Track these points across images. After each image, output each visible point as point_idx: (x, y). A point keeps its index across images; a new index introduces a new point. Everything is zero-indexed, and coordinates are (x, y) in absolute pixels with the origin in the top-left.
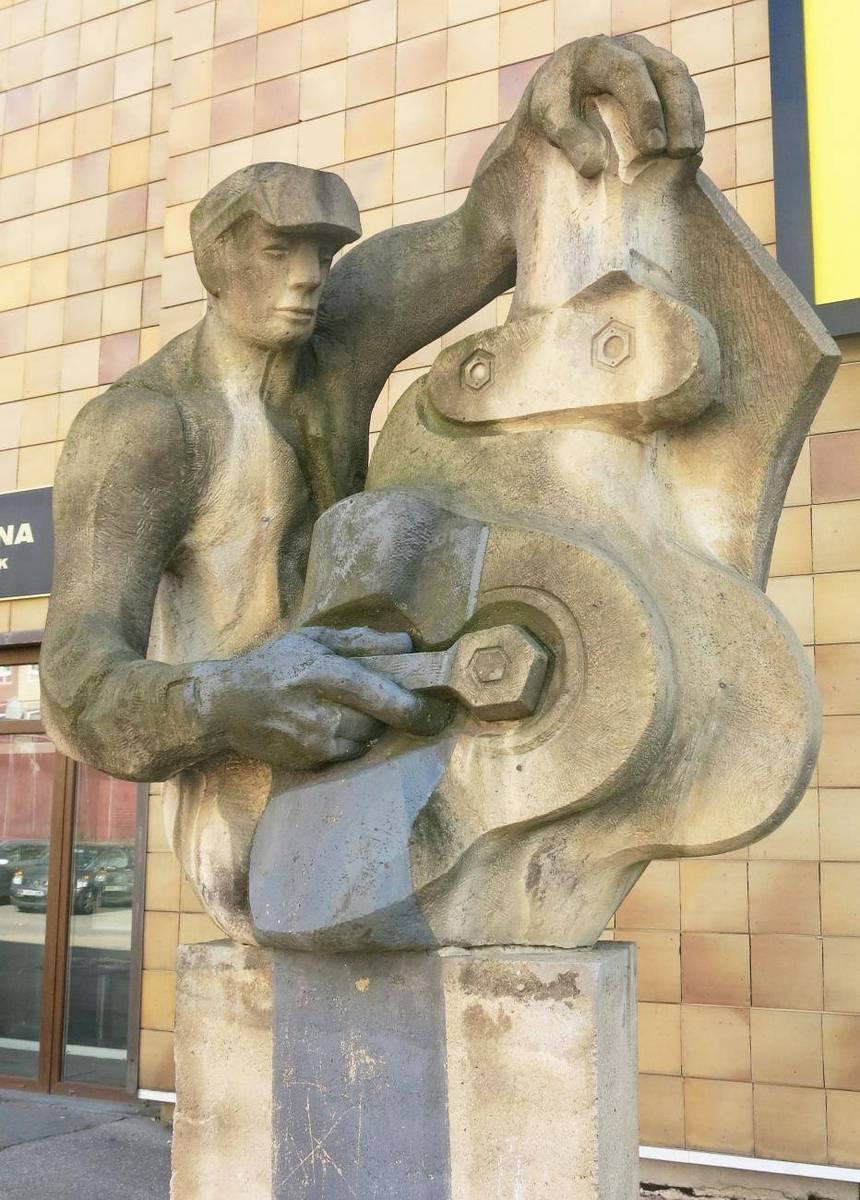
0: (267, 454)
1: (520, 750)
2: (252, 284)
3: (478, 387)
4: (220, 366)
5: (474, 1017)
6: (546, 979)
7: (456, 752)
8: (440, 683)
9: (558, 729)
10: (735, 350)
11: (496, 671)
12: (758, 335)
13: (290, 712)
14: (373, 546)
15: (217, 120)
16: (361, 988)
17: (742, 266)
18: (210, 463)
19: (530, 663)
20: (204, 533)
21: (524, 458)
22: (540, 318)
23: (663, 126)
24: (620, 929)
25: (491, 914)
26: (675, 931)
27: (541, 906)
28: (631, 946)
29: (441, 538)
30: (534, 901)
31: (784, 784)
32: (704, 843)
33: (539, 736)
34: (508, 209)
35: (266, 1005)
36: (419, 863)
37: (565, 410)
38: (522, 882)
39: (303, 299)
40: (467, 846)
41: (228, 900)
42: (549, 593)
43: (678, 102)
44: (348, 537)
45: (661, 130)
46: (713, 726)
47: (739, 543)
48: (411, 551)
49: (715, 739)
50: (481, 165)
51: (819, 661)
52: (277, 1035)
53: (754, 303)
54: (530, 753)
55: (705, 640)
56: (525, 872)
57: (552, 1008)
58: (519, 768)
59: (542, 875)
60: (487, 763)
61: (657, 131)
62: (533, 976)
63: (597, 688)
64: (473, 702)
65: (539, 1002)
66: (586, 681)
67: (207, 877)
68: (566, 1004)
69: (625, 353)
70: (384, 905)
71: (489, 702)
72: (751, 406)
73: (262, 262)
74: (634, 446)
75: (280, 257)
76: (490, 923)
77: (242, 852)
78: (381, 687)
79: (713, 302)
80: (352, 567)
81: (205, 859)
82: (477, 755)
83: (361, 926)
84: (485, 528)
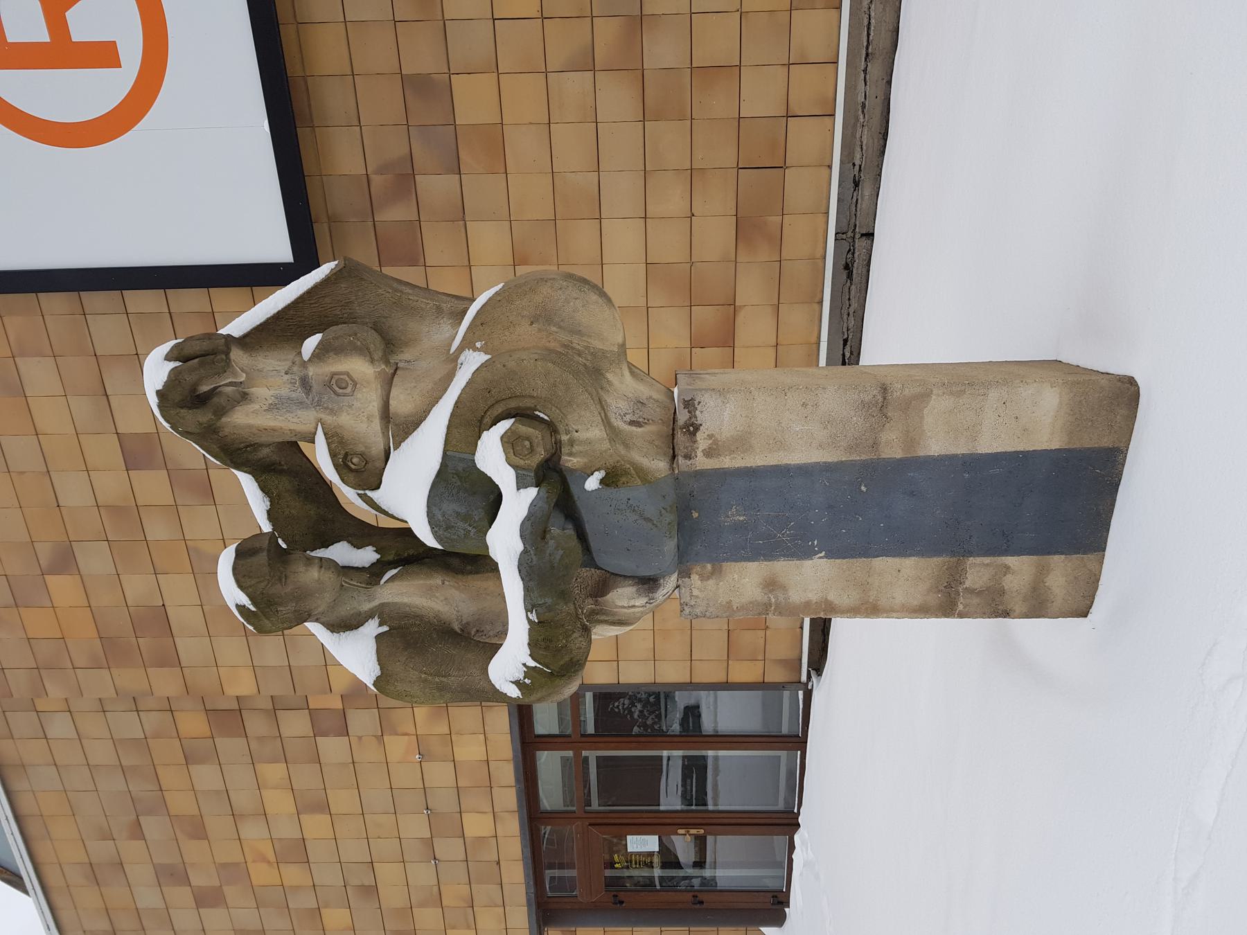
0: (405, 583)
1: (568, 432)
2: (302, 595)
5: (708, 453)
7: (570, 466)
8: (532, 474)
10: (341, 316)
14: (458, 514)
15: (162, 663)
16: (697, 515)
17: (291, 312)
19: (520, 426)
25: (656, 446)
30: (650, 424)
34: (256, 446)
35: (709, 566)
38: (639, 430)
41: (653, 588)
44: (453, 529)
49: (560, 327)
51: (524, 262)
52: (727, 560)
53: (314, 305)
55: (507, 333)
58: (577, 432)
60: (576, 448)
64: (542, 456)
67: (641, 601)
79: (313, 328)
82: (570, 454)
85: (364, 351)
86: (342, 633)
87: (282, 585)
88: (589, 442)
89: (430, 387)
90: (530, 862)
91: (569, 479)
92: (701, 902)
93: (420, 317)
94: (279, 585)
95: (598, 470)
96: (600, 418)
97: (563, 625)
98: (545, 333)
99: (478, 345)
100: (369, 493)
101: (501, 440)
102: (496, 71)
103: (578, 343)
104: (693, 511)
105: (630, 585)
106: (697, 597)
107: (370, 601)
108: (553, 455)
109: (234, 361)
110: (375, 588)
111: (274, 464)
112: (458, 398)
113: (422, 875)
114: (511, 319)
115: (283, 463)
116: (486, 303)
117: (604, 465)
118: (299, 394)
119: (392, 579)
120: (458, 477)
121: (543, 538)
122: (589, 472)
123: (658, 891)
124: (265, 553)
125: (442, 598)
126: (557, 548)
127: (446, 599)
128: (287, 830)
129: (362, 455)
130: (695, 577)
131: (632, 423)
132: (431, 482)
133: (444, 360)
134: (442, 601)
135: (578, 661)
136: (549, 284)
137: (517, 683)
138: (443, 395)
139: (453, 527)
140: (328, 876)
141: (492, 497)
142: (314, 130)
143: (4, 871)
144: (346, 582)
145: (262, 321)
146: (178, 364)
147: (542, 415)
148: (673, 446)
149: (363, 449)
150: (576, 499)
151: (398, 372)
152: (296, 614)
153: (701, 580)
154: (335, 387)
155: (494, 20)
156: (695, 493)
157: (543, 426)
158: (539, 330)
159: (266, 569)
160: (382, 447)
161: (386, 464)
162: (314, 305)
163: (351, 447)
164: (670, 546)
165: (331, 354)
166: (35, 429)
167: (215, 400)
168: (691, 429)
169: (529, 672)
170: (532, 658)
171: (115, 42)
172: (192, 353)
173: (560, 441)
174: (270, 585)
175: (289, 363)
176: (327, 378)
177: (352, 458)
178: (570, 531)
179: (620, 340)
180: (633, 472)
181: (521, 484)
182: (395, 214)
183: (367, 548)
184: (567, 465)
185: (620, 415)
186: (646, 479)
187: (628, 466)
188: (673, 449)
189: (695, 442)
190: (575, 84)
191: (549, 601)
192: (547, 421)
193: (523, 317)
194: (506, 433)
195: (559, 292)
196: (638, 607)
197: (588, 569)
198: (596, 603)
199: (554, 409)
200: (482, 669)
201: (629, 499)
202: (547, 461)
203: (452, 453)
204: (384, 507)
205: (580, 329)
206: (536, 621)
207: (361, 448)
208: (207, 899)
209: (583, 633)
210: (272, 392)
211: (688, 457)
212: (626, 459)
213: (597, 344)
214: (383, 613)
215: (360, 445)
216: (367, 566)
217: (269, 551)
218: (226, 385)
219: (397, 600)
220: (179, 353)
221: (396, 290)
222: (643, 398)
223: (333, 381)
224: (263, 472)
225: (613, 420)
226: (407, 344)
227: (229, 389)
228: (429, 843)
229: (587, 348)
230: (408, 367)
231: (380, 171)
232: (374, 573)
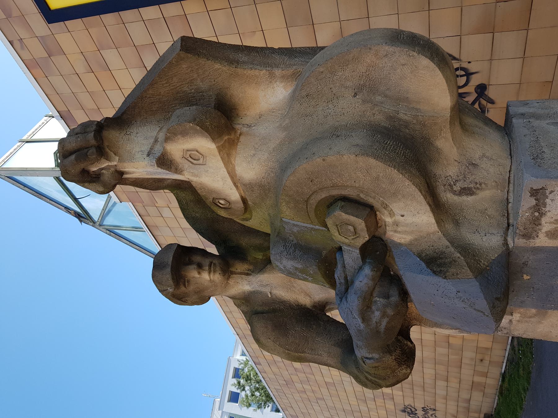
1: (392, 214)
3: (228, 203)
4: (239, 292)
6: (533, 202)
8: (358, 251)
9: (379, 199)
10: (190, 92)
11: (349, 228)
12: (180, 82)
13: (376, 322)
14: (296, 269)
17: (151, 92)
19: (343, 214)
20: (306, 301)
21: (253, 191)
22: (192, 182)
23: (87, 150)
24: (494, 29)
26: (496, 4)
27: (485, 184)
28: (512, 110)
31: (413, 56)
32: (449, 98)
33: (384, 208)
36: (457, 274)
37: (229, 173)
38: (470, 199)
39: (204, 270)
40: (448, 243)
43: (75, 144)
45: (88, 151)
46: (379, 98)
47: (284, 78)
48: (297, 251)
49: (386, 96)
54: (393, 211)
56: (465, 198)
57: (552, 200)
59: (466, 186)
61: (88, 154)
62: (530, 208)
68: (550, 193)
70: (482, 295)
71: (366, 232)
72: (214, 81)
73: (191, 288)
74: (242, 139)
75: (188, 281)
78: (361, 282)
82: (396, 231)
83: (494, 304)
156: (530, 262)
162: (160, 88)
166: (120, 88)
211: (527, 236)
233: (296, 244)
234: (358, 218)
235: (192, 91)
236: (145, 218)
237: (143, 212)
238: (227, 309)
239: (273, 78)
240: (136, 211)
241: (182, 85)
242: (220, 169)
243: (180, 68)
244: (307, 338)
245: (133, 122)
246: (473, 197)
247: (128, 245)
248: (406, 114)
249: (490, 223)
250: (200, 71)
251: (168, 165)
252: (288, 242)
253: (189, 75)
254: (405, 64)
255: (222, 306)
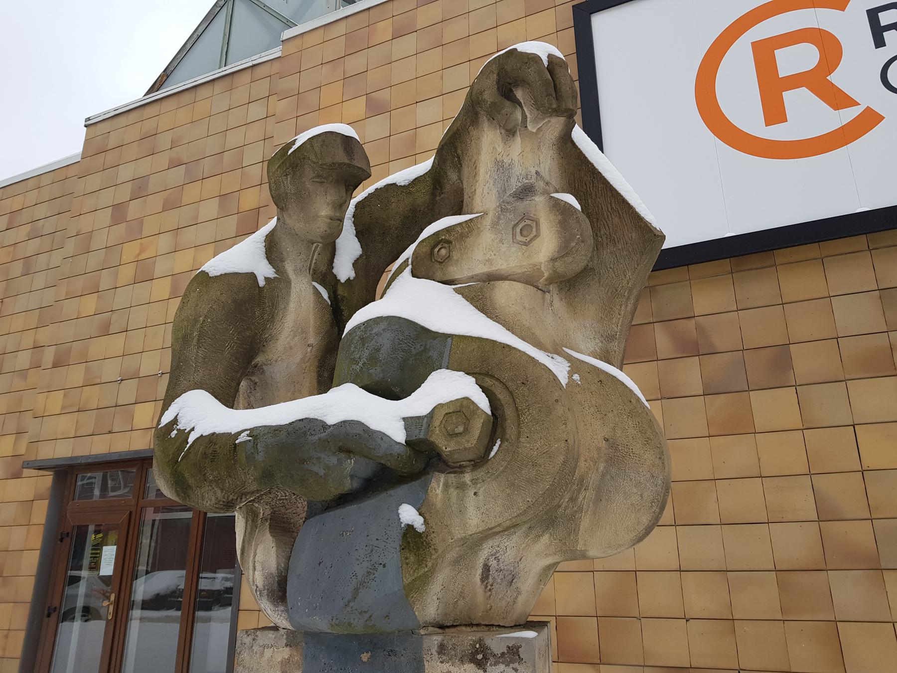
0: (312, 305)
1: (474, 482)
2: (303, 199)
7: (432, 484)
8: (422, 436)
10: (599, 234)
14: (378, 350)
17: (601, 186)
18: (276, 309)
29: (421, 345)
30: (485, 592)
34: (459, 166)
38: (478, 578)
41: (273, 595)
42: (492, 376)
43: (563, 82)
48: (402, 353)
50: (440, 144)
55: (592, 409)
58: (475, 494)
60: (453, 492)
63: (528, 437)
65: (493, 667)
66: (519, 432)
68: (513, 669)
69: (534, 233)
76: (456, 608)
77: (283, 560)
80: (364, 364)
81: (258, 567)
82: (446, 486)
84: (449, 338)
85: (564, 251)
86: (264, 244)
87: (313, 178)
88: (462, 510)
89: (525, 323)
90: (108, 459)
91: (415, 485)
92: (49, 615)
93: (601, 318)
94: (314, 175)
95: (426, 522)
96: (493, 526)
97: (230, 476)
98: (596, 456)
99: (576, 377)
100: (409, 269)
101: (464, 398)
102: (804, 427)
103: (586, 497)
104: (369, 654)
105: (278, 564)
106: (262, 654)
107: (294, 271)
108: (446, 463)
109: (549, 121)
110: (310, 277)
111: (441, 188)
112: (514, 348)
113: (111, 371)
114: (610, 415)
115: (442, 196)
116: (627, 387)
117: (432, 530)
118: (515, 185)
119: (317, 293)
120: (422, 351)
121: (341, 450)
122: (423, 510)
123: (66, 572)
124: (346, 161)
125: (292, 344)
126: (327, 467)
127: (291, 348)
128: (161, 267)
129: (449, 257)
130: (285, 653)
131: (486, 568)
132: (416, 321)
133: (554, 341)
134: (289, 343)
135: (189, 496)
136: (657, 461)
137: (175, 421)
138: (517, 336)
139: (364, 345)
140: (121, 299)
141: (397, 390)
142: (729, 273)
143: (161, 84)
144: (316, 248)
145: (590, 159)
146: (546, 64)
147: (496, 448)
148: (456, 626)
149: (455, 258)
150: (389, 492)
151: (540, 292)
152: (284, 195)
153: (282, 662)
154: (523, 224)
155: (854, 426)
156: (394, 659)
157: (482, 450)
158: (599, 449)
159: (329, 160)
160: (456, 277)
161: (439, 282)
163: (458, 246)
164: (321, 624)
165: (560, 217)
167: (507, 103)
168: (480, 657)
169: (184, 435)
170: (198, 439)
171: (885, 46)
172: (557, 76)
173: (462, 472)
174: (313, 165)
175: (547, 178)
176: (532, 215)
177: (445, 248)
178: (349, 485)
179: (591, 553)
180: (422, 571)
181: (410, 423)
182: (662, 339)
183: (353, 272)
184: (433, 480)
185: (497, 552)
186: (411, 590)
187: (430, 564)
188: (453, 626)
189: (462, 661)
190: (806, 506)
191: (260, 457)
192: (489, 455)
193: (614, 429)
194: (473, 403)
195: (648, 476)
196: (254, 574)
197: (306, 509)
198: (264, 519)
199: (505, 464)
200: (200, 382)
201: (384, 566)
202: (439, 456)
203: (450, 343)
204: (393, 284)
205: (603, 500)
206: (237, 442)
207: (456, 255)
208: (119, 212)
209: (221, 503)
210: (516, 159)
212: (440, 561)
213: (585, 522)
214: (279, 283)
215: (459, 255)
216: (334, 271)
217: (349, 165)
218: (523, 113)
219: (293, 296)
220: (556, 65)
221: (630, 291)
222: (517, 583)
223: (528, 222)
224: (435, 177)
225: (490, 543)
226: (570, 304)
227: (518, 116)
228: (135, 376)
229: (580, 510)
230: (546, 304)
231: (699, 328)
232: (326, 277)
233: (411, 352)
234: (477, 439)
235: (599, 238)
236: (249, 73)
237: (259, 72)
238: (46, 180)
239: (606, 340)
240: (265, 60)
241: (609, 227)
242: (507, 261)
243: (632, 229)
244: (221, 352)
245: (562, 153)
246: (479, 580)
247: (195, 32)
248: (584, 498)
249: (449, 604)
250: (625, 253)
251: (519, 195)
252: (414, 343)
253: (621, 239)
254: (642, 498)
255: (52, 173)
